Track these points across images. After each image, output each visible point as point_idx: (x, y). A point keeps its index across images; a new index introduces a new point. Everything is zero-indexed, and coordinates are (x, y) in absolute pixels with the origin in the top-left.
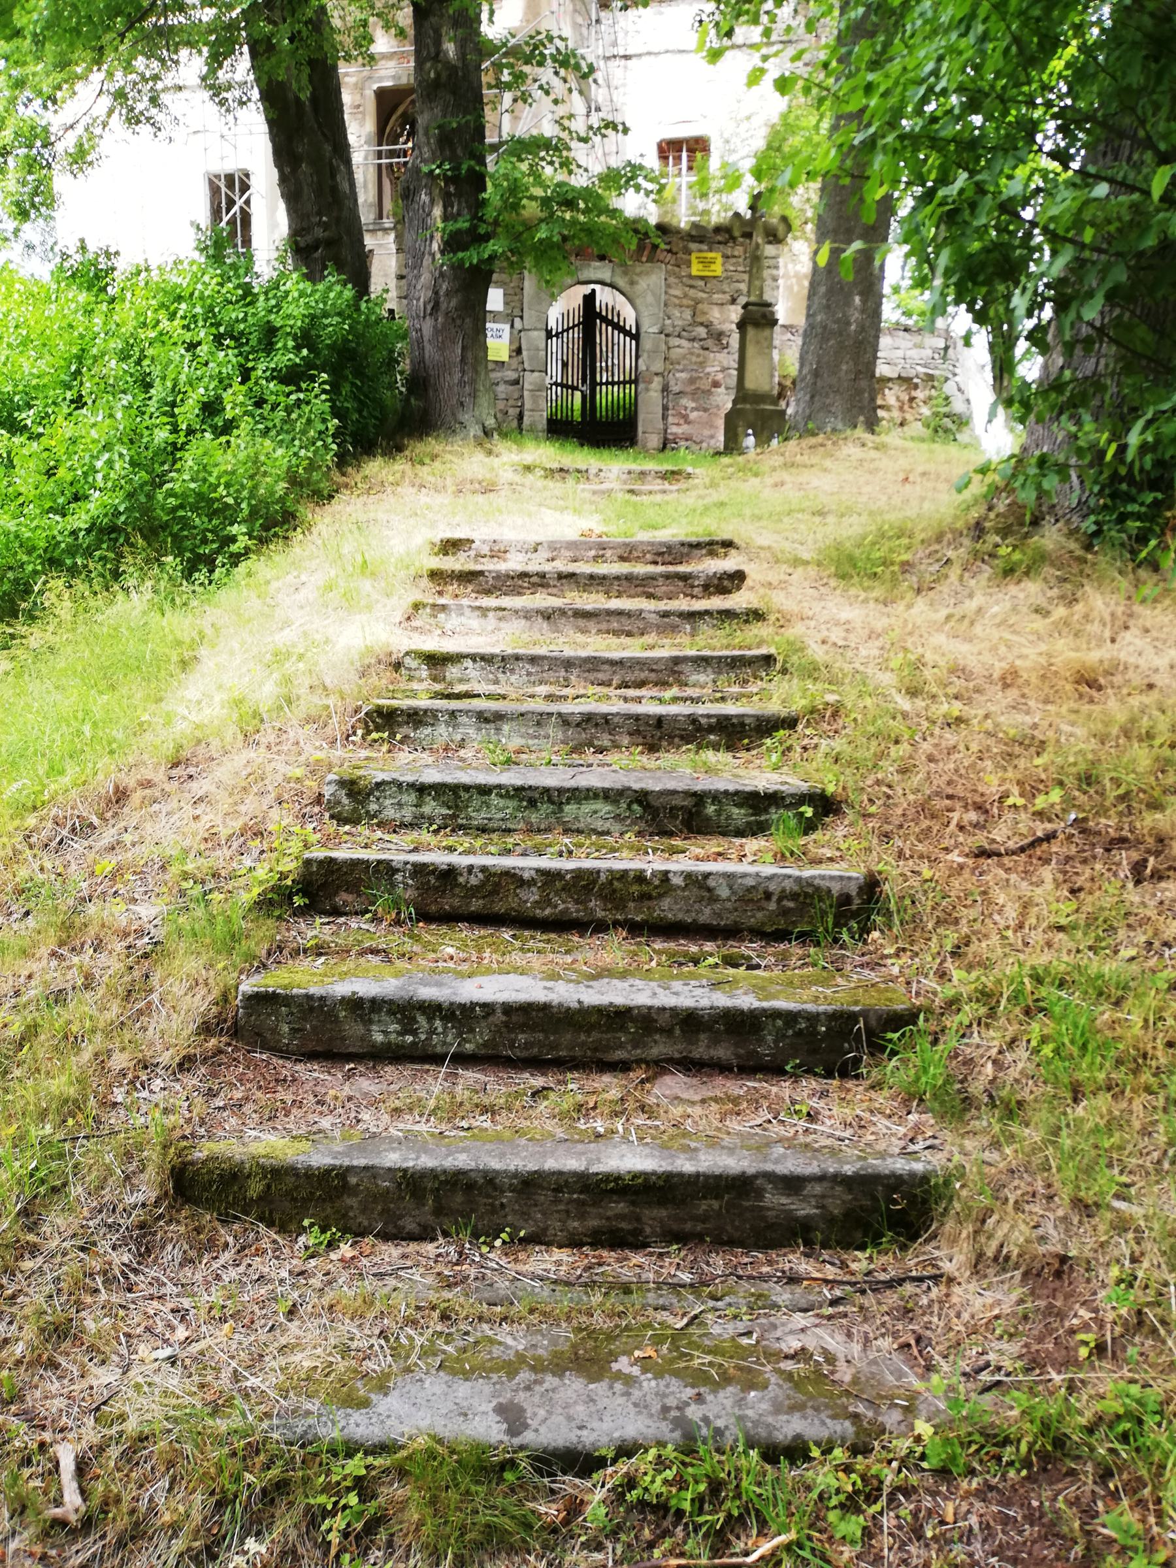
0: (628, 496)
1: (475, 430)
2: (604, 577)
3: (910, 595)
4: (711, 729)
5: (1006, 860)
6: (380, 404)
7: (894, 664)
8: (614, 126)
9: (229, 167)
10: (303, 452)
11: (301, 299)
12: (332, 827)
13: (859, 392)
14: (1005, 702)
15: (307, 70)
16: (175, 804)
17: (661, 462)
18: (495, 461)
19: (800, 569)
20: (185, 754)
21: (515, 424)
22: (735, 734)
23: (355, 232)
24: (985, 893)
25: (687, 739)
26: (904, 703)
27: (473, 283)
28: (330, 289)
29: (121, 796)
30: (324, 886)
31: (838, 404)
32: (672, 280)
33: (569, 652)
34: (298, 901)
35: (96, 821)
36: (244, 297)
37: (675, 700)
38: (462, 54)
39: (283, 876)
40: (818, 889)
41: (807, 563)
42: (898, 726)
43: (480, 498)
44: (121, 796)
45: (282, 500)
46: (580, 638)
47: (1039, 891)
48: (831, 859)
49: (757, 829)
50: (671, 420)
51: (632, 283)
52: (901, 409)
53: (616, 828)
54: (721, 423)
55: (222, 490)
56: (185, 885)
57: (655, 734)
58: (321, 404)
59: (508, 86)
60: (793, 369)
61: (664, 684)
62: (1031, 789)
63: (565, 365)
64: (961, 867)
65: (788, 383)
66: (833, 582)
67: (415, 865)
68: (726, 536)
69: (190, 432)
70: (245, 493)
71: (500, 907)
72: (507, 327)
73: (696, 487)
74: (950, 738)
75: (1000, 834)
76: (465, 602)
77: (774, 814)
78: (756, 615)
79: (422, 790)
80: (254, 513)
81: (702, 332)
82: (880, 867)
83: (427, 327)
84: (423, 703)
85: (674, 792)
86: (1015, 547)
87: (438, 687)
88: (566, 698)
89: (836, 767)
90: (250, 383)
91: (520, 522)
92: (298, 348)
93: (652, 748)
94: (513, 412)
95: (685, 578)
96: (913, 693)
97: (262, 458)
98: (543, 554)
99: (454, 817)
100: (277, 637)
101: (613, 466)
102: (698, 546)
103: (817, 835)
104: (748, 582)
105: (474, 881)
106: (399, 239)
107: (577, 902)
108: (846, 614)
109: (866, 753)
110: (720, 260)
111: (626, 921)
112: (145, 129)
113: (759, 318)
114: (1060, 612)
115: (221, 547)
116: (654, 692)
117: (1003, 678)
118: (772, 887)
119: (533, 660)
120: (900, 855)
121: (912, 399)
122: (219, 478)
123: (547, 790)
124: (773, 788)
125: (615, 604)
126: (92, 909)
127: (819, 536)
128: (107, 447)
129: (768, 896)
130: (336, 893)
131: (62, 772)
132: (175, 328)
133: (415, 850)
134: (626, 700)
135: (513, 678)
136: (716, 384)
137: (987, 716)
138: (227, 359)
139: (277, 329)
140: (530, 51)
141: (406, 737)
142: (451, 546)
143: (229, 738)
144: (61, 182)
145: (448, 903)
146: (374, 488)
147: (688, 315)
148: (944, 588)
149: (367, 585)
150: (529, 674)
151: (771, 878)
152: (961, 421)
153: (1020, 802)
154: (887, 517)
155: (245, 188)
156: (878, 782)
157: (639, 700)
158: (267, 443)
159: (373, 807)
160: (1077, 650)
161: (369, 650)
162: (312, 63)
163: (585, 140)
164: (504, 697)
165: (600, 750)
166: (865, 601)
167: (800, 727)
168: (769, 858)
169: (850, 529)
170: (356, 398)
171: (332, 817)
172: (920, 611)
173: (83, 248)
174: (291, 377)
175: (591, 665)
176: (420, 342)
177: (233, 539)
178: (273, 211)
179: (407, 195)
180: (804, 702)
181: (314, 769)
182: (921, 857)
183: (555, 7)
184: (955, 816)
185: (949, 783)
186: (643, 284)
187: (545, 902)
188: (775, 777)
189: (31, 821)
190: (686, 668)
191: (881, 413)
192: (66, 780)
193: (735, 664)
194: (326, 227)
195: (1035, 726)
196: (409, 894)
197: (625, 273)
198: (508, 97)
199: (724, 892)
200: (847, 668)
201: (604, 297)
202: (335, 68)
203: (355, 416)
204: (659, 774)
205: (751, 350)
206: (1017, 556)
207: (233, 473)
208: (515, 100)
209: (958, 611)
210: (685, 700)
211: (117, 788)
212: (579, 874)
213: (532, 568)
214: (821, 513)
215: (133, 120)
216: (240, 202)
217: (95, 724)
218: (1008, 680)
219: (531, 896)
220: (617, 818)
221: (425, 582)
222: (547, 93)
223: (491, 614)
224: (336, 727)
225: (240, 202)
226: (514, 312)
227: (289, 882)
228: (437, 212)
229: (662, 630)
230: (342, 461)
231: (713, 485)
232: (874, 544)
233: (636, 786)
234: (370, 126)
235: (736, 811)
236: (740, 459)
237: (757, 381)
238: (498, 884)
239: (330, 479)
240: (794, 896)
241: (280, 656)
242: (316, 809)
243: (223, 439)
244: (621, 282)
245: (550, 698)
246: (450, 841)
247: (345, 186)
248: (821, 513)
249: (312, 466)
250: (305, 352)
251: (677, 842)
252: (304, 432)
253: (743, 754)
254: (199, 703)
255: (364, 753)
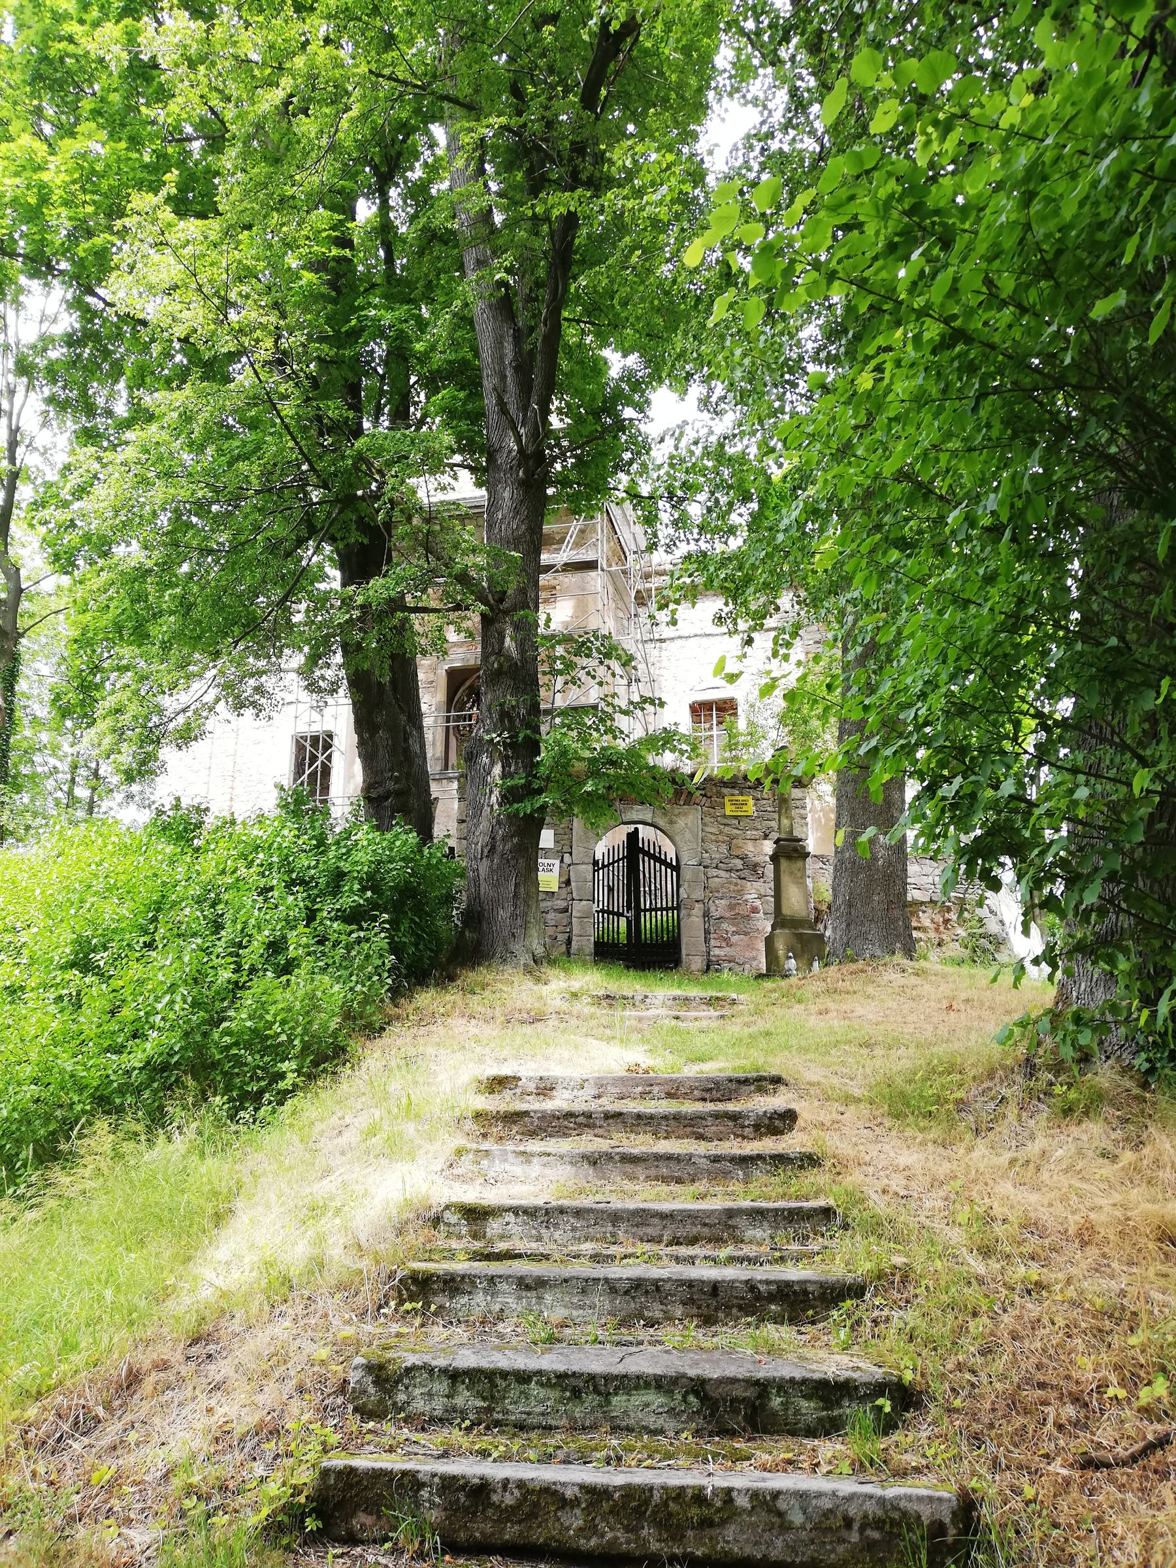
0: (674, 1022)
1: (525, 959)
2: (652, 1117)
3: (968, 1136)
4: (771, 1298)
5: (1117, 1472)
6: (434, 934)
7: (962, 1218)
8: (652, 702)
9: (317, 728)
10: (358, 988)
11: (368, 846)
12: (353, 1423)
13: (893, 921)
14: (1084, 1265)
15: (390, 662)
16: (189, 1393)
17: (704, 985)
18: (545, 990)
19: (852, 1108)
20: (207, 1328)
21: (563, 948)
22: (799, 1304)
23: (421, 782)
24: (1098, 1520)
25: (747, 1309)
26: (977, 1266)
27: (529, 827)
28: (397, 836)
29: (134, 1379)
30: (339, 1505)
31: (874, 932)
32: (707, 819)
33: (617, 1204)
34: (311, 1524)
35: (100, 1411)
36: (317, 847)
37: (731, 1260)
38: (522, 646)
39: (297, 1491)
40: (905, 1514)
41: (859, 1101)
42: (972, 1294)
43: (528, 1029)
44: (134, 1379)
45: (335, 1035)
46: (629, 1186)
47: (1161, 1516)
48: (917, 1470)
49: (830, 1428)
50: (713, 942)
51: (671, 822)
52: (937, 930)
53: (670, 1425)
54: (762, 946)
55: (277, 1028)
56: (188, 1503)
57: (711, 1304)
58: (380, 941)
59: (560, 672)
60: (828, 896)
61: (718, 1241)
62: (1133, 1380)
63: (611, 890)
64: (1067, 1482)
65: (824, 908)
66: (888, 1122)
67: (443, 1478)
68: (774, 1072)
69: (253, 970)
70: (299, 1030)
71: (538, 1536)
72: (557, 862)
73: (741, 1013)
74: (1033, 1309)
75: (1108, 1435)
76: (510, 1146)
77: (848, 1409)
78: (810, 1161)
79: (454, 1376)
80: (306, 1047)
81: (738, 863)
82: (974, 1483)
83: (484, 867)
84: (461, 1266)
85: (733, 1381)
86: (1070, 1085)
87: (478, 1245)
88: (613, 1258)
89: (911, 1347)
90: (315, 924)
91: (566, 1055)
92: (363, 889)
93: (708, 1321)
94: (562, 937)
95: (734, 1117)
96: (986, 1252)
97: (319, 994)
98: (590, 1090)
99: (489, 1410)
100: (316, 1187)
101: (658, 992)
102: (746, 1082)
103: (897, 1436)
104: (800, 1122)
105: (509, 1500)
106: (461, 789)
107: (628, 1529)
108: (907, 1158)
109: (943, 1329)
110: (751, 802)
111: (685, 1556)
112: (249, 713)
113: (790, 851)
114: (1128, 1156)
115: (270, 1084)
116: (708, 1250)
117: (1080, 1235)
118: (852, 1511)
119: (578, 1213)
120: (995, 1465)
121: (946, 921)
122: (275, 1015)
123: (592, 1377)
124: (846, 1374)
125: (665, 1146)
126: (81, 1532)
127: (868, 1071)
128: (172, 988)
129: (848, 1522)
130: (353, 1515)
131: (74, 1348)
132: (251, 875)
133: (445, 1455)
134: (677, 1259)
135: (557, 1235)
136: (755, 910)
137: (1069, 1282)
138: (294, 903)
139: (345, 874)
140: (580, 644)
141: (441, 1307)
142: (498, 1083)
143: (254, 1310)
144: (167, 753)
145: (481, 1529)
146: (425, 1019)
147: (724, 848)
148: (1003, 1128)
149: (410, 1128)
150: (574, 1229)
151: (852, 1497)
152: (999, 942)
153: (1122, 1393)
154: (935, 1050)
155: (328, 746)
156: (960, 1367)
157: (691, 1260)
158: (326, 979)
159: (401, 1397)
160: (1154, 1201)
161: (408, 1203)
162: (393, 657)
163: (626, 713)
164: (547, 1257)
165: (651, 1323)
166: (923, 1143)
167: (868, 1296)
168: (846, 1468)
169: (901, 1062)
170: (414, 933)
171: (356, 1410)
172: (981, 1155)
173: (177, 807)
174: (354, 917)
175: (640, 1218)
176: (476, 881)
177: (282, 1076)
178: (350, 764)
179: (470, 758)
180: (868, 1266)
181: (342, 1349)
182: (1020, 1467)
183: (600, 607)
184: (1050, 1410)
185: (1039, 1367)
186: (681, 823)
187: (590, 1529)
188: (844, 1359)
189: (32, 1412)
190: (741, 1222)
191: (915, 934)
192: (77, 1359)
193: (793, 1216)
194: (397, 780)
195: (1123, 1294)
196: (434, 1516)
197: (665, 814)
198: (560, 680)
199: (797, 1518)
200: (913, 1224)
201: (646, 833)
202: (414, 659)
203: (411, 950)
204: (717, 1355)
205: (785, 879)
206: (1073, 1095)
207: (289, 1009)
208: (566, 683)
209: (1021, 1155)
210: (741, 1260)
211: (130, 1370)
212: (630, 1491)
213: (579, 1107)
214: (867, 1045)
215: (239, 706)
216: (321, 758)
217: (118, 1287)
218: (1086, 1237)
219: (574, 1520)
220: (672, 1412)
221: (469, 1125)
222: (594, 677)
223: (535, 1160)
224: (368, 1296)
225: (321, 758)
226: (563, 849)
227: (302, 1499)
228: (497, 770)
229: (713, 1176)
230: (396, 992)
231: (758, 1012)
232: (925, 1079)
233: (692, 1372)
234: (441, 696)
235: (804, 1404)
236: (783, 983)
237: (795, 902)
238: (536, 1505)
239: (381, 1009)
240: (878, 1524)
241: (315, 1211)
242: (340, 1400)
243: (284, 979)
244: (661, 822)
245: (596, 1258)
246: (483, 1443)
247: (417, 748)
248: (867, 1045)
249: (366, 1000)
250: (369, 894)
251: (740, 1445)
252: (361, 968)
253: (808, 1328)
254: (228, 1265)
255: (395, 1328)
